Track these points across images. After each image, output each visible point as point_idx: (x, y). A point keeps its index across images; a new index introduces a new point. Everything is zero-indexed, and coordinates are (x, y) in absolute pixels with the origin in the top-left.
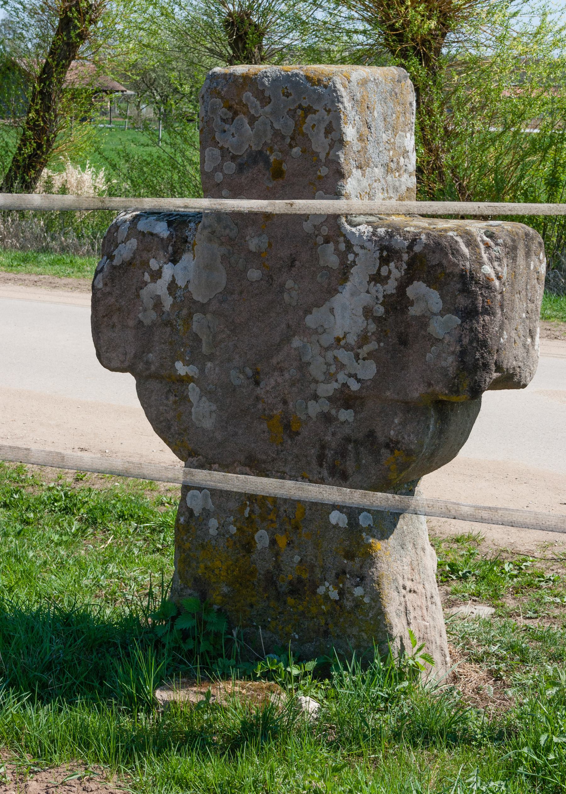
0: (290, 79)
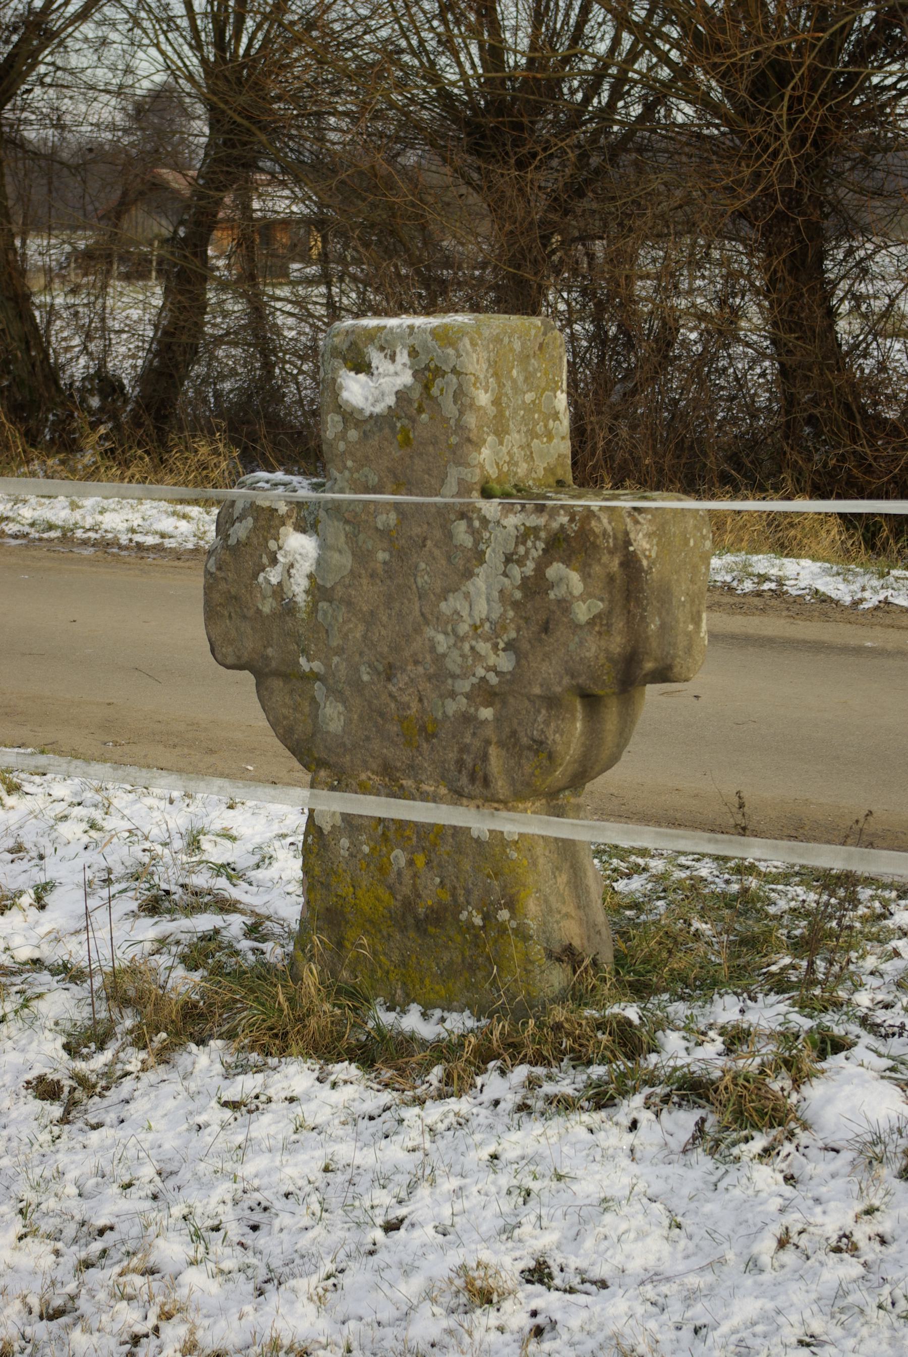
0: (699, 495)
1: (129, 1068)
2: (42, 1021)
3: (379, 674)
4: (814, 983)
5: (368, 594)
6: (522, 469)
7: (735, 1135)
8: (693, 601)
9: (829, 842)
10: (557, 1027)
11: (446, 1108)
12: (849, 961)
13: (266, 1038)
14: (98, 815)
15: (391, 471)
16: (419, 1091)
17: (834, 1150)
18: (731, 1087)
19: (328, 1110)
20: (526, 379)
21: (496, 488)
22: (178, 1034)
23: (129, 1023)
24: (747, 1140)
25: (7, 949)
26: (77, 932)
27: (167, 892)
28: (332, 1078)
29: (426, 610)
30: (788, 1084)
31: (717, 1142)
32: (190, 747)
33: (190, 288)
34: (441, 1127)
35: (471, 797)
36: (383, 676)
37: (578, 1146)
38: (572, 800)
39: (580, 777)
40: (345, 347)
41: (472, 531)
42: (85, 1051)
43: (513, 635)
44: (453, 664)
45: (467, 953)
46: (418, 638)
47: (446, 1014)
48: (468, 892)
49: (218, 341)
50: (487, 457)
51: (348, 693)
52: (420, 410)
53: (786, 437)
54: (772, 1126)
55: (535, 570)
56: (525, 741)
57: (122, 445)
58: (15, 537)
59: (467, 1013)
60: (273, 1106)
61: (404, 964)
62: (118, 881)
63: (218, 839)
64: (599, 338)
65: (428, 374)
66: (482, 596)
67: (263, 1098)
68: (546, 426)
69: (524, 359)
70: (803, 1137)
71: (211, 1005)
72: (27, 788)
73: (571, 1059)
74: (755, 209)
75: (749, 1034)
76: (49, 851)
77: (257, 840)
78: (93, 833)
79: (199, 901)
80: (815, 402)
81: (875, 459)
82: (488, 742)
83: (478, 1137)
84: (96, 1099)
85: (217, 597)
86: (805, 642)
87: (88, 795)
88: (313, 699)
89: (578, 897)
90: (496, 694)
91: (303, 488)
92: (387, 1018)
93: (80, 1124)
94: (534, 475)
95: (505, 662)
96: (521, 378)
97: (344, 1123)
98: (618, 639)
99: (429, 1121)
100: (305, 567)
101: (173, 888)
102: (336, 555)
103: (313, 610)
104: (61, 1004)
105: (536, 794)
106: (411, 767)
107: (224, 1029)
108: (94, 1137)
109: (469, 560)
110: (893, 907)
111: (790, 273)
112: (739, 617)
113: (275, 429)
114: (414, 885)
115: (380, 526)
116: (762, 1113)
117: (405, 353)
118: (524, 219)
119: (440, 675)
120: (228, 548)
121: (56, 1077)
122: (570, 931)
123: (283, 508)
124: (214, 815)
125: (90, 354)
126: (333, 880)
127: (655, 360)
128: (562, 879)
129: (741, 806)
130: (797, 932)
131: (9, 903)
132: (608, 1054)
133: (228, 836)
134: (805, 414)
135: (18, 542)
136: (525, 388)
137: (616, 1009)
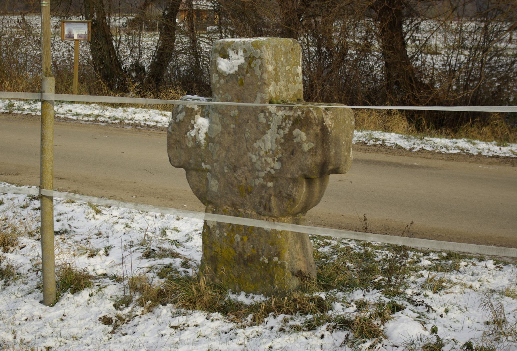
1: (137, 313)
2: (106, 296)
3: (231, 170)
4: (392, 285)
5: (227, 140)
6: (284, 95)
7: (359, 341)
8: (347, 144)
9: (398, 235)
10: (295, 300)
11: (253, 330)
12: (404, 278)
13: (188, 303)
14: (129, 222)
15: (236, 95)
16: (243, 323)
17: (396, 346)
18: (359, 323)
19: (210, 330)
20: (286, 61)
21: (275, 101)
22: (155, 301)
23: (137, 297)
24: (364, 342)
25: (94, 270)
26: (120, 264)
27: (154, 250)
28: (212, 318)
29: (248, 146)
30: (380, 322)
31: (353, 343)
32: (163, 198)
33: (169, 33)
34: (251, 336)
35: (264, 215)
36: (232, 171)
37: (301, 344)
38: (302, 217)
39: (305, 209)
40: (220, 49)
41: (266, 117)
42: (121, 307)
43: (280, 155)
44: (258, 166)
45: (262, 273)
46: (246, 157)
47: (254, 295)
48: (263, 250)
49: (179, 52)
50: (271, 90)
51: (219, 176)
52: (247, 72)
53: (387, 89)
54: (373, 338)
55: (289, 131)
56: (284, 195)
57: (143, 90)
58: (103, 122)
59: (262, 295)
60: (190, 328)
61: (239, 277)
62: (135, 246)
63: (173, 231)
64: (319, 53)
65: (250, 59)
66: (269, 141)
67: (186, 325)
68: (294, 79)
69: (286, 54)
70: (385, 342)
71: (168, 291)
72: (103, 212)
73: (300, 312)
74: (376, 6)
75: (366, 304)
76: (110, 235)
77: (187, 232)
78: (127, 228)
79: (165, 253)
80: (398, 76)
81: (420, 97)
82: (271, 195)
83: (265, 340)
84: (125, 324)
85: (172, 141)
86: (392, 163)
87: (126, 215)
88: (207, 179)
89: (304, 253)
90: (274, 177)
91: (203, 101)
92: (232, 297)
93: (119, 334)
94: (289, 97)
95: (277, 166)
96: (285, 61)
97: (216, 335)
98: (319, 157)
99: (247, 334)
100: (204, 130)
101: (155, 249)
102: (216, 126)
103: (207, 146)
104: (113, 290)
105: (288, 214)
106: (242, 204)
107: (172, 300)
108: (124, 338)
109: (264, 128)
110: (421, 259)
111: (389, 29)
112: (368, 154)
113: (197, 82)
114: (243, 248)
115: (232, 115)
116: (370, 332)
117: (242, 51)
118: (291, 8)
119: (253, 169)
120: (176, 123)
121: (110, 316)
122: (301, 265)
123: (196, 108)
124: (171, 222)
125: (133, 57)
126: (213, 246)
127: (339, 60)
128: (298, 246)
129: (365, 220)
130: (385, 267)
131: (95, 253)
132: (313, 310)
133: (176, 230)
134: (394, 81)
135: (104, 124)
136: (286, 65)
137: (317, 294)
